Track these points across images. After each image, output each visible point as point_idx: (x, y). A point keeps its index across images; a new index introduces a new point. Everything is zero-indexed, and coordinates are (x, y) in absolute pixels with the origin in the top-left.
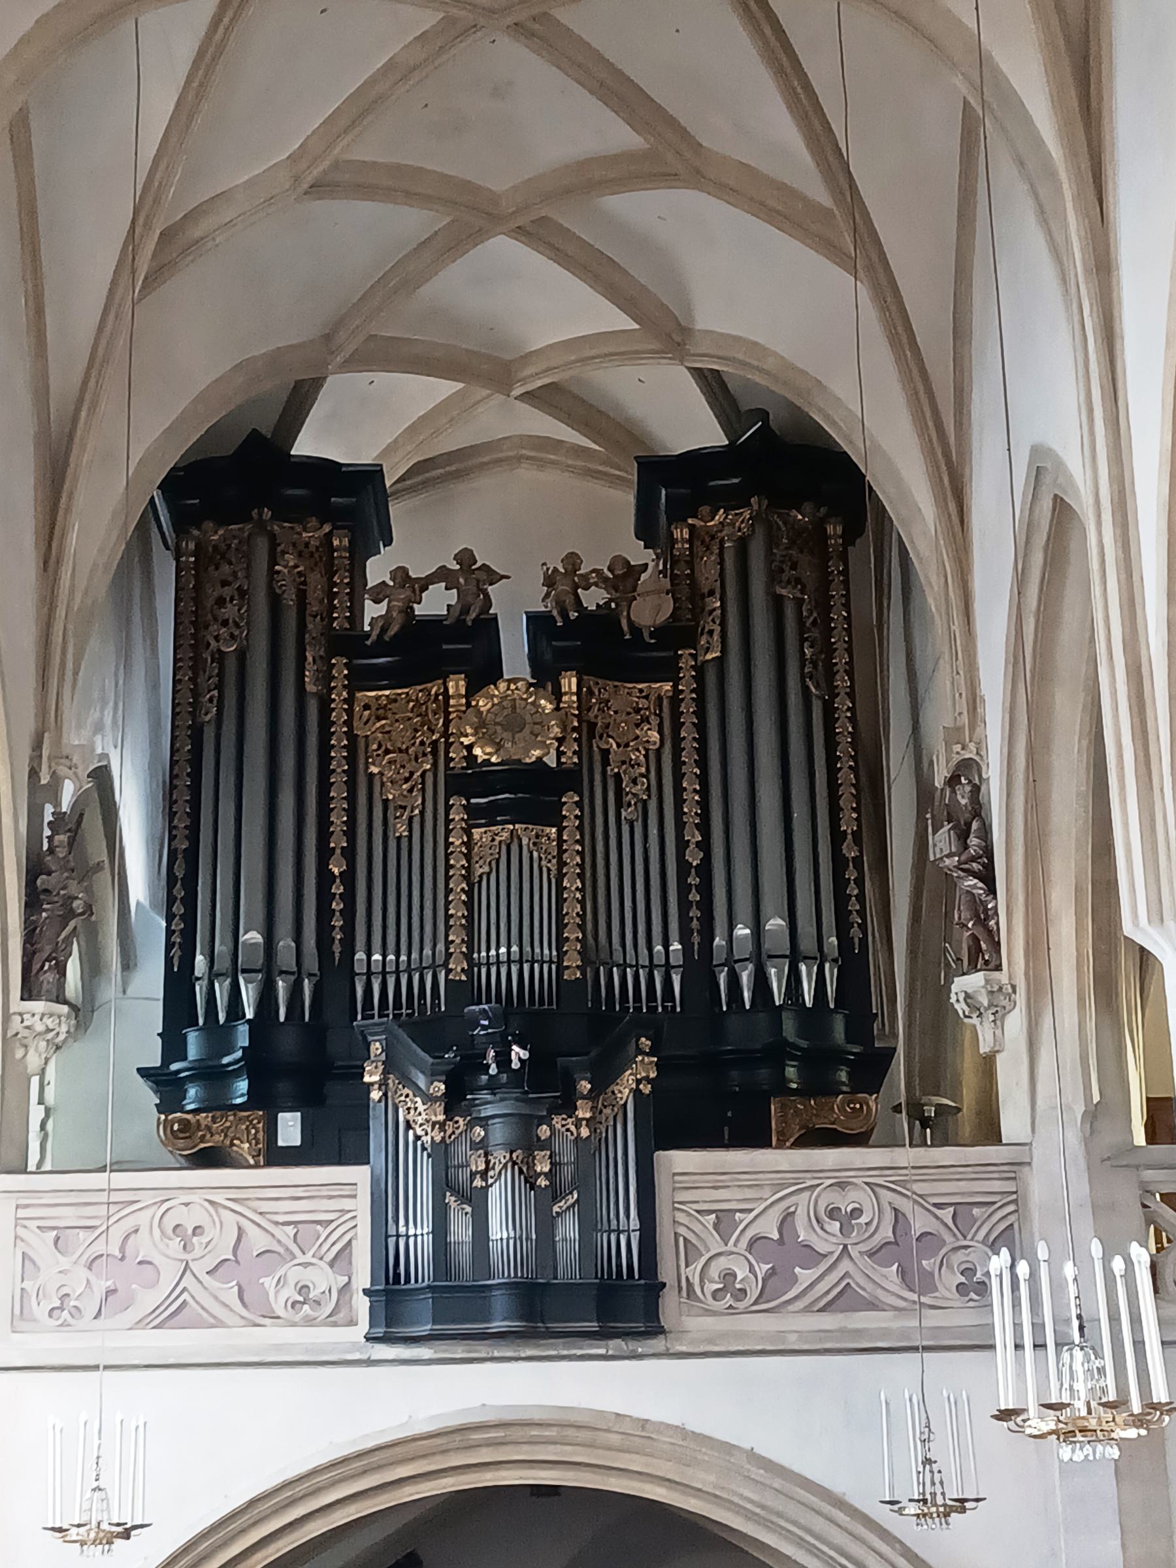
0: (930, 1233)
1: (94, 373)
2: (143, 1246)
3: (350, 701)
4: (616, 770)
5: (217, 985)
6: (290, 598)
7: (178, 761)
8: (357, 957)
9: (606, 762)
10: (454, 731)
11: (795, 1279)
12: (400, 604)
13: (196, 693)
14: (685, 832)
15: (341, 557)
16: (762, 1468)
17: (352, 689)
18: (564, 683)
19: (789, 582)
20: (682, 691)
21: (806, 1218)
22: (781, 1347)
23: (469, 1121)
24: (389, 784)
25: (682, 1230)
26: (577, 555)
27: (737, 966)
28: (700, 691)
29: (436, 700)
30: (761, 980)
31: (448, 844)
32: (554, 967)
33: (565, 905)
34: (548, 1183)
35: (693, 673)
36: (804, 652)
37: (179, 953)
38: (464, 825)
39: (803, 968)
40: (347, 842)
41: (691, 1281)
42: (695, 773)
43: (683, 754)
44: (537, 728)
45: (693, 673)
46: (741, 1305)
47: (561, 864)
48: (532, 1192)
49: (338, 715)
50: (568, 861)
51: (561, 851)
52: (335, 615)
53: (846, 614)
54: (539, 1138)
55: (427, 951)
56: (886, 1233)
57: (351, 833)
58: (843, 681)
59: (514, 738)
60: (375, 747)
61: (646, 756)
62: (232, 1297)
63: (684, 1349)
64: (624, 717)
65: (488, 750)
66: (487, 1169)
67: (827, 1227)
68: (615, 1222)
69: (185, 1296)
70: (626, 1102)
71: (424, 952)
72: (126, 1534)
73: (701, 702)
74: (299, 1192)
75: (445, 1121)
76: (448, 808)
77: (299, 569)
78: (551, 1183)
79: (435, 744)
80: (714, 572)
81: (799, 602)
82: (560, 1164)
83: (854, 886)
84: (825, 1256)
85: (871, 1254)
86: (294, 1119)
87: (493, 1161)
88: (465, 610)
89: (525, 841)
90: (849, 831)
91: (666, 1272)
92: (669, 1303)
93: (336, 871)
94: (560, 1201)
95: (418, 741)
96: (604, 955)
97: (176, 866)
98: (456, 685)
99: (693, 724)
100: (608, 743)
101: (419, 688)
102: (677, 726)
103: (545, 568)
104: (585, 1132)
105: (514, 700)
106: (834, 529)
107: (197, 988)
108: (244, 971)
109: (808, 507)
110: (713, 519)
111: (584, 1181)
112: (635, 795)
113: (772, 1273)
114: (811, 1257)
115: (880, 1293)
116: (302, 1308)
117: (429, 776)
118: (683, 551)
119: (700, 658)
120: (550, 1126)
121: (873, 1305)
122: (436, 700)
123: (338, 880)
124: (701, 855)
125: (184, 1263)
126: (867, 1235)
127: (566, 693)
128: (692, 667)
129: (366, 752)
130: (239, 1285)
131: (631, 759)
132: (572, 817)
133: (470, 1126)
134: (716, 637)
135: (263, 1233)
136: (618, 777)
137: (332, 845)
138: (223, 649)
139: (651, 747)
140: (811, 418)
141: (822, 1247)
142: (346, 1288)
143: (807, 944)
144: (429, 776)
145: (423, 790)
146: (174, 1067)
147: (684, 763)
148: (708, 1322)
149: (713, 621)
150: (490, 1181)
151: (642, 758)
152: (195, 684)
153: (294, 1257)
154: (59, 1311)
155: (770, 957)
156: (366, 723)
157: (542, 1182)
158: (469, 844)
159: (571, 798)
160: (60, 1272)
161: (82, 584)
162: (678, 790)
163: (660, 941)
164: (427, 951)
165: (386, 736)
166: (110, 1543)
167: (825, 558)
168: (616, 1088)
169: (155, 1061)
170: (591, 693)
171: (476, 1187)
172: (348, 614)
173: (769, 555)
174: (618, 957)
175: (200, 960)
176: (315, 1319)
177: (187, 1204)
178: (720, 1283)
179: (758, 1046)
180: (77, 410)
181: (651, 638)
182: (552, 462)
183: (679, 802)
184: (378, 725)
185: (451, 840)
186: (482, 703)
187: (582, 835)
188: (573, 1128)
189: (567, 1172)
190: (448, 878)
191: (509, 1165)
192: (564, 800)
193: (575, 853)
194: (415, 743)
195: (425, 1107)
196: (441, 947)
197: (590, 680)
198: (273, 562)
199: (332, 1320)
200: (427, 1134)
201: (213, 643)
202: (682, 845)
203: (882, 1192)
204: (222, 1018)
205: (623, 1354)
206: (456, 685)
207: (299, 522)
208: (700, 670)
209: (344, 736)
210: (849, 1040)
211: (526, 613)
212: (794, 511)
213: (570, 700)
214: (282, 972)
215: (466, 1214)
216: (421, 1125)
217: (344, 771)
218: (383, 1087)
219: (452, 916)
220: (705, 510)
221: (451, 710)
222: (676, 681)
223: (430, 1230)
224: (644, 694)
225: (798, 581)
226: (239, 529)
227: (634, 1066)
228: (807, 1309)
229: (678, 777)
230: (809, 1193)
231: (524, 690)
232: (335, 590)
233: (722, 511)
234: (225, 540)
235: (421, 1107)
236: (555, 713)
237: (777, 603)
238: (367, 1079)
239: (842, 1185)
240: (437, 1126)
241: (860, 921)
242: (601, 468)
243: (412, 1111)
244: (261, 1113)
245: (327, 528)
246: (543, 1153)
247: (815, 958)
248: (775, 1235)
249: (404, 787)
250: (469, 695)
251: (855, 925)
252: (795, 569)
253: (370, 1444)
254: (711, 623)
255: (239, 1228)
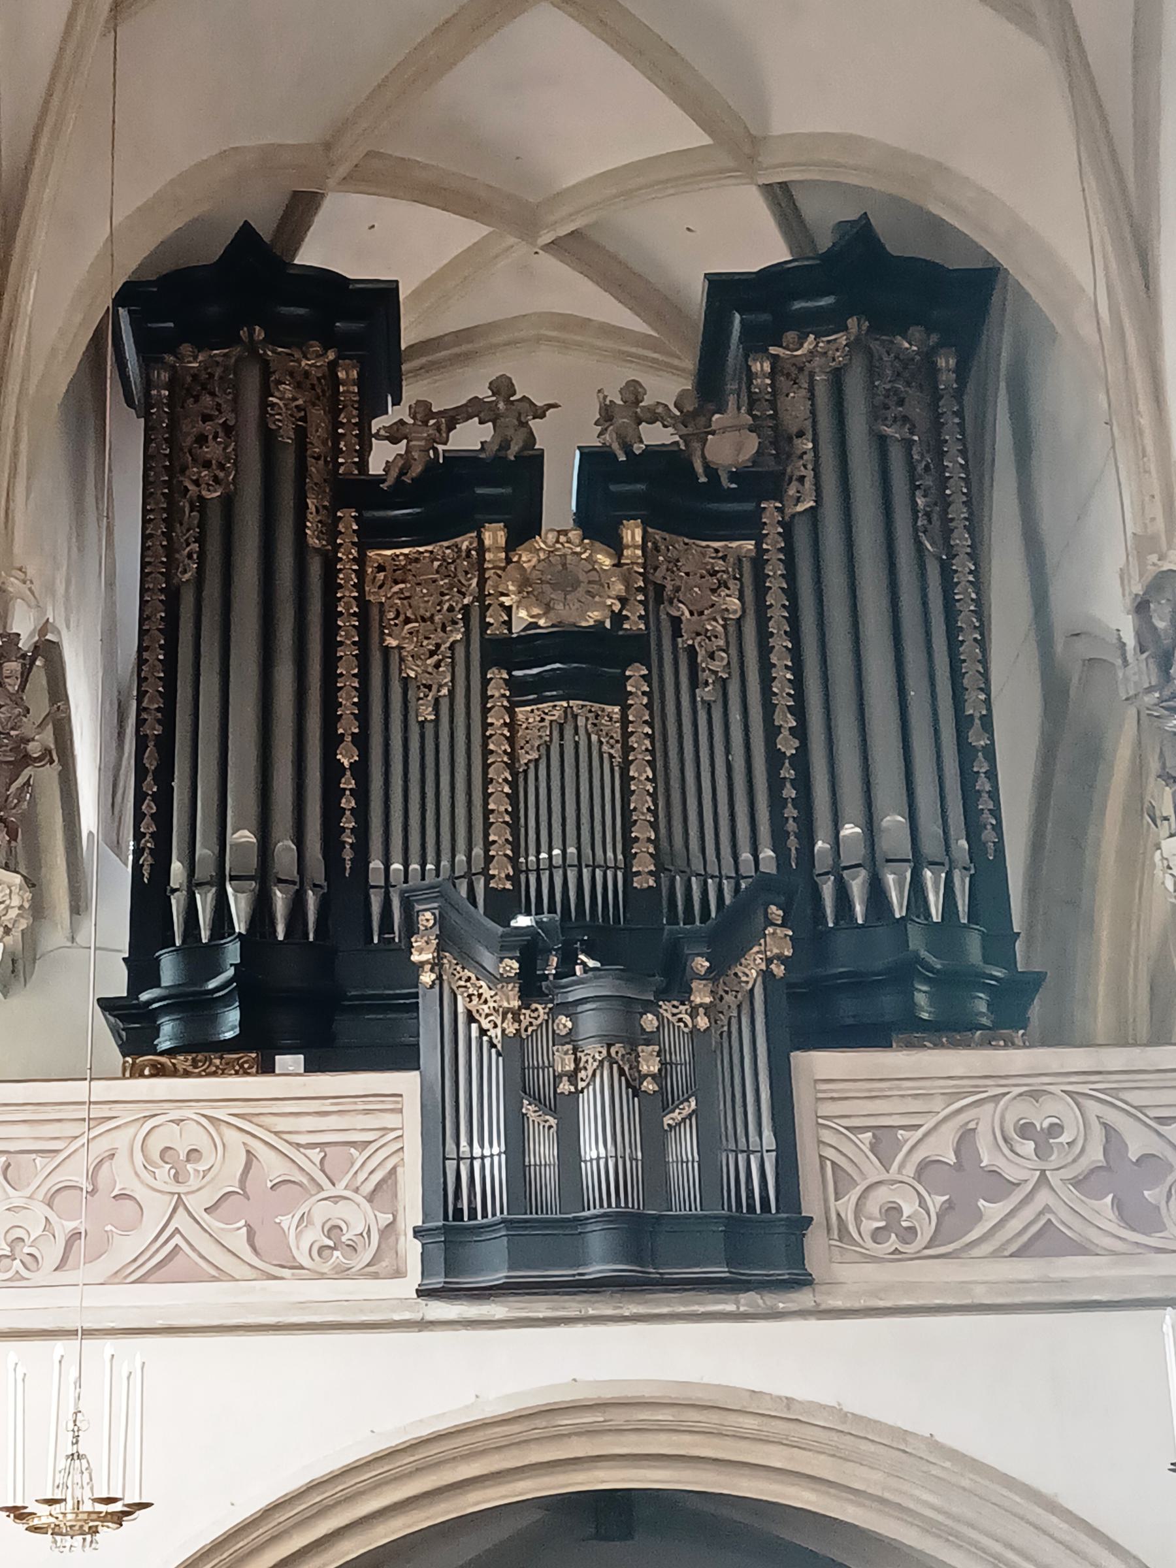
0: (1154, 1156)
1: (59, 86)
2: (121, 1176)
3: (361, 560)
4: (690, 642)
5: (198, 896)
6: (287, 436)
7: (148, 630)
8: (371, 866)
9: (677, 633)
10: (491, 592)
11: (979, 1216)
12: (423, 443)
13: (170, 550)
14: (775, 717)
15: (349, 391)
16: (949, 1460)
17: (362, 547)
18: (627, 537)
19: (895, 420)
20: (767, 550)
21: (992, 1137)
22: (968, 1301)
23: (550, 1009)
24: (410, 659)
25: (829, 1153)
26: (637, 382)
27: (845, 873)
28: (789, 552)
29: (468, 555)
30: (877, 893)
31: (486, 725)
32: (620, 874)
33: (633, 798)
34: (656, 1089)
35: (780, 530)
36: (917, 502)
37: (150, 860)
38: (506, 703)
39: (928, 874)
40: (359, 727)
41: (843, 1215)
42: (786, 647)
43: (770, 624)
44: (594, 588)
45: (780, 530)
46: (910, 1249)
47: (627, 749)
48: (636, 1099)
49: (347, 575)
50: (636, 745)
51: (626, 735)
52: (341, 460)
53: (963, 462)
54: (643, 1029)
55: (461, 857)
56: (1096, 1155)
57: (363, 717)
58: (962, 538)
59: (565, 599)
60: (391, 615)
61: (724, 627)
62: (239, 1241)
63: (838, 1303)
64: (699, 581)
65: (536, 611)
66: (577, 1070)
67: (1018, 1149)
68: (744, 1140)
69: (177, 1239)
70: (752, 990)
71: (457, 859)
72: (118, 1518)
73: (790, 562)
74: (326, 1106)
75: (520, 1008)
76: (485, 682)
77: (297, 403)
78: (661, 1088)
79: (466, 609)
80: (803, 408)
81: (909, 444)
82: (671, 1063)
83: (986, 780)
84: (1018, 1185)
85: (1077, 1183)
86: (296, 1063)
87: (584, 1059)
88: (505, 445)
89: (581, 722)
90: (977, 715)
91: (811, 1206)
92: (816, 1244)
93: (346, 764)
94: (673, 1111)
95: (446, 606)
96: (681, 863)
97: (147, 755)
98: (494, 535)
99: (782, 589)
100: (678, 609)
101: (446, 544)
102: (761, 591)
103: (601, 395)
104: (703, 1022)
105: (565, 555)
106: (946, 362)
107: (173, 902)
108: (232, 878)
109: (916, 332)
110: (801, 346)
111: (700, 1087)
112: (715, 673)
113: (948, 1207)
114: (999, 1187)
115: (1092, 1234)
116: (332, 1255)
117: (460, 651)
118: (763, 387)
119: (789, 511)
120: (658, 1016)
121: (1082, 1249)
122: (468, 555)
123: (348, 773)
124: (797, 743)
125: (176, 1196)
126: (1070, 1159)
127: (628, 547)
128: (779, 522)
129: (381, 621)
130: (247, 1225)
131: (707, 630)
132: (640, 694)
133: (553, 1013)
134: (808, 483)
135: (280, 1158)
136: (692, 652)
137: (341, 731)
138: (204, 493)
139: (731, 616)
140: (929, 213)
141: (1012, 1173)
142: (389, 1230)
143: (931, 847)
144: (460, 651)
145: (453, 665)
146: (145, 997)
147: (772, 634)
148: (870, 1271)
149: (805, 466)
150: (581, 1085)
151: (720, 629)
152: (170, 539)
153: (321, 1188)
154: (8, 1261)
155: (888, 861)
156: (380, 587)
157: (649, 1086)
158: (512, 726)
159: (636, 672)
160: (8, 1209)
161: (38, 368)
162: (766, 667)
163: (748, 849)
164: (461, 857)
165: (405, 602)
166: (94, 1531)
167: (936, 396)
168: (739, 969)
169: (118, 987)
170: (656, 549)
171: (562, 1093)
172: (357, 460)
173: (871, 388)
174: (697, 865)
175: (177, 868)
176: (349, 1269)
177: (177, 1122)
178: (882, 1220)
179: (879, 965)
180: (36, 137)
181: (731, 481)
182: (580, 345)
183: (767, 680)
184: (396, 588)
185: (490, 720)
186: (526, 557)
187: (651, 715)
188: (687, 1018)
189: (680, 1077)
190: (486, 767)
191: (606, 1064)
192: (628, 673)
193: (643, 736)
194: (442, 608)
195: (493, 993)
196: (478, 851)
197: (658, 535)
198: (266, 392)
199: (370, 1272)
200: (496, 1026)
201: (191, 487)
202: (772, 731)
203: (1089, 1104)
204: (205, 937)
205: (760, 1311)
206: (494, 535)
207: (300, 347)
208: (788, 527)
209: (354, 603)
210: (986, 960)
211: (579, 448)
212: (899, 338)
213: (633, 554)
214: (280, 881)
215: (550, 1127)
216: (487, 1015)
217: (354, 643)
218: (437, 968)
219: (492, 811)
220: (791, 336)
221: (486, 565)
222: (760, 539)
223: (503, 1149)
224: (720, 554)
225: (905, 419)
226: (225, 355)
227: (762, 941)
228: (996, 1254)
229: (764, 650)
230: (992, 1105)
231: (577, 541)
232: (340, 431)
233: (812, 337)
234: (206, 369)
235: (487, 993)
236: (618, 570)
237: (881, 442)
238: (415, 958)
239: (1035, 1095)
240: (510, 1016)
241: (994, 822)
242: (633, 350)
243: (475, 1000)
244: (254, 1055)
245: (331, 355)
246: (650, 1048)
247: (942, 864)
248: (951, 1159)
249: (429, 662)
250: (511, 546)
251: (989, 827)
252: (902, 405)
253: (425, 1432)
254: (802, 468)
255: (248, 1152)
